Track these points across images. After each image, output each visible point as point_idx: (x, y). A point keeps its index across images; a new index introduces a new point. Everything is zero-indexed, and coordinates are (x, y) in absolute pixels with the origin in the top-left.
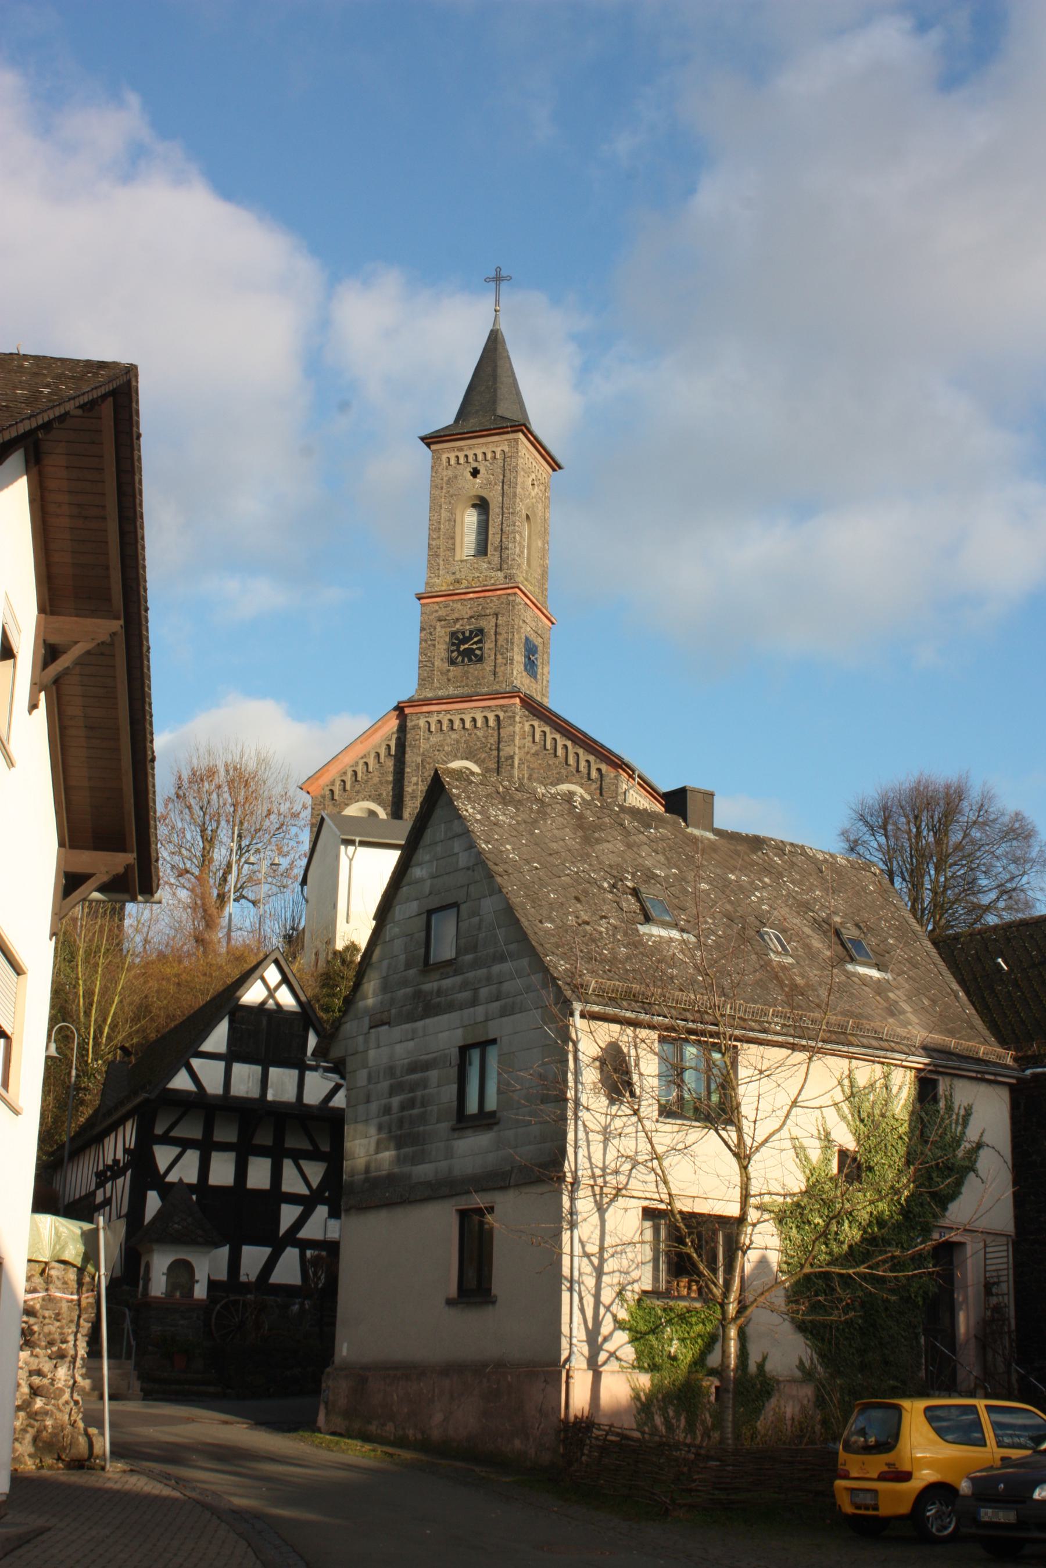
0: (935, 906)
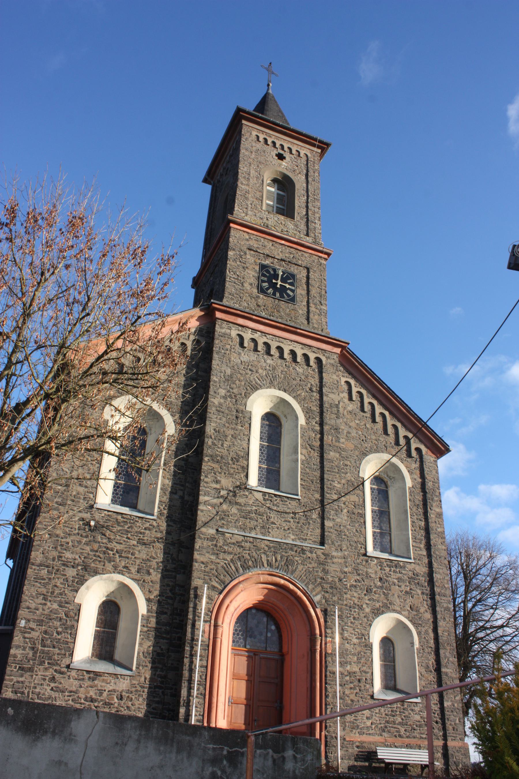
0: (66, 628)
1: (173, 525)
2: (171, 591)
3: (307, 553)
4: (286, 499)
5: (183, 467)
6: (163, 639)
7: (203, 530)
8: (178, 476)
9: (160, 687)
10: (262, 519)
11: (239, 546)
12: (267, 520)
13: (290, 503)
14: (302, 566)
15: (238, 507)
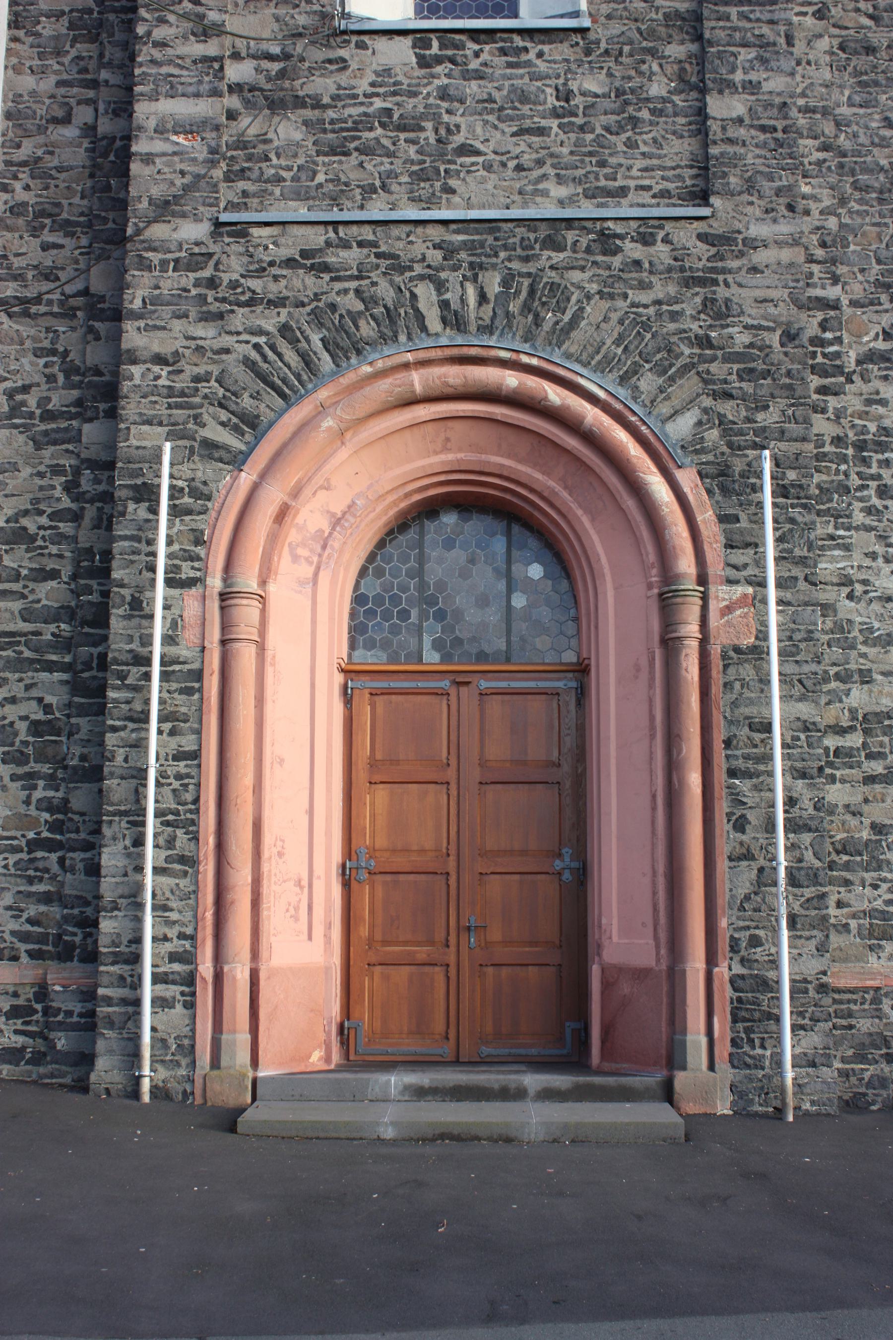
1: (60, 241)
2: (68, 488)
3: (628, 245)
4: (519, 42)
5: (90, 11)
6: (51, 671)
7: (158, 231)
8: (73, 53)
9: (50, 846)
10: (414, 142)
11: (312, 267)
12: (439, 141)
13: (540, 55)
14: (605, 305)
15: (308, 113)
